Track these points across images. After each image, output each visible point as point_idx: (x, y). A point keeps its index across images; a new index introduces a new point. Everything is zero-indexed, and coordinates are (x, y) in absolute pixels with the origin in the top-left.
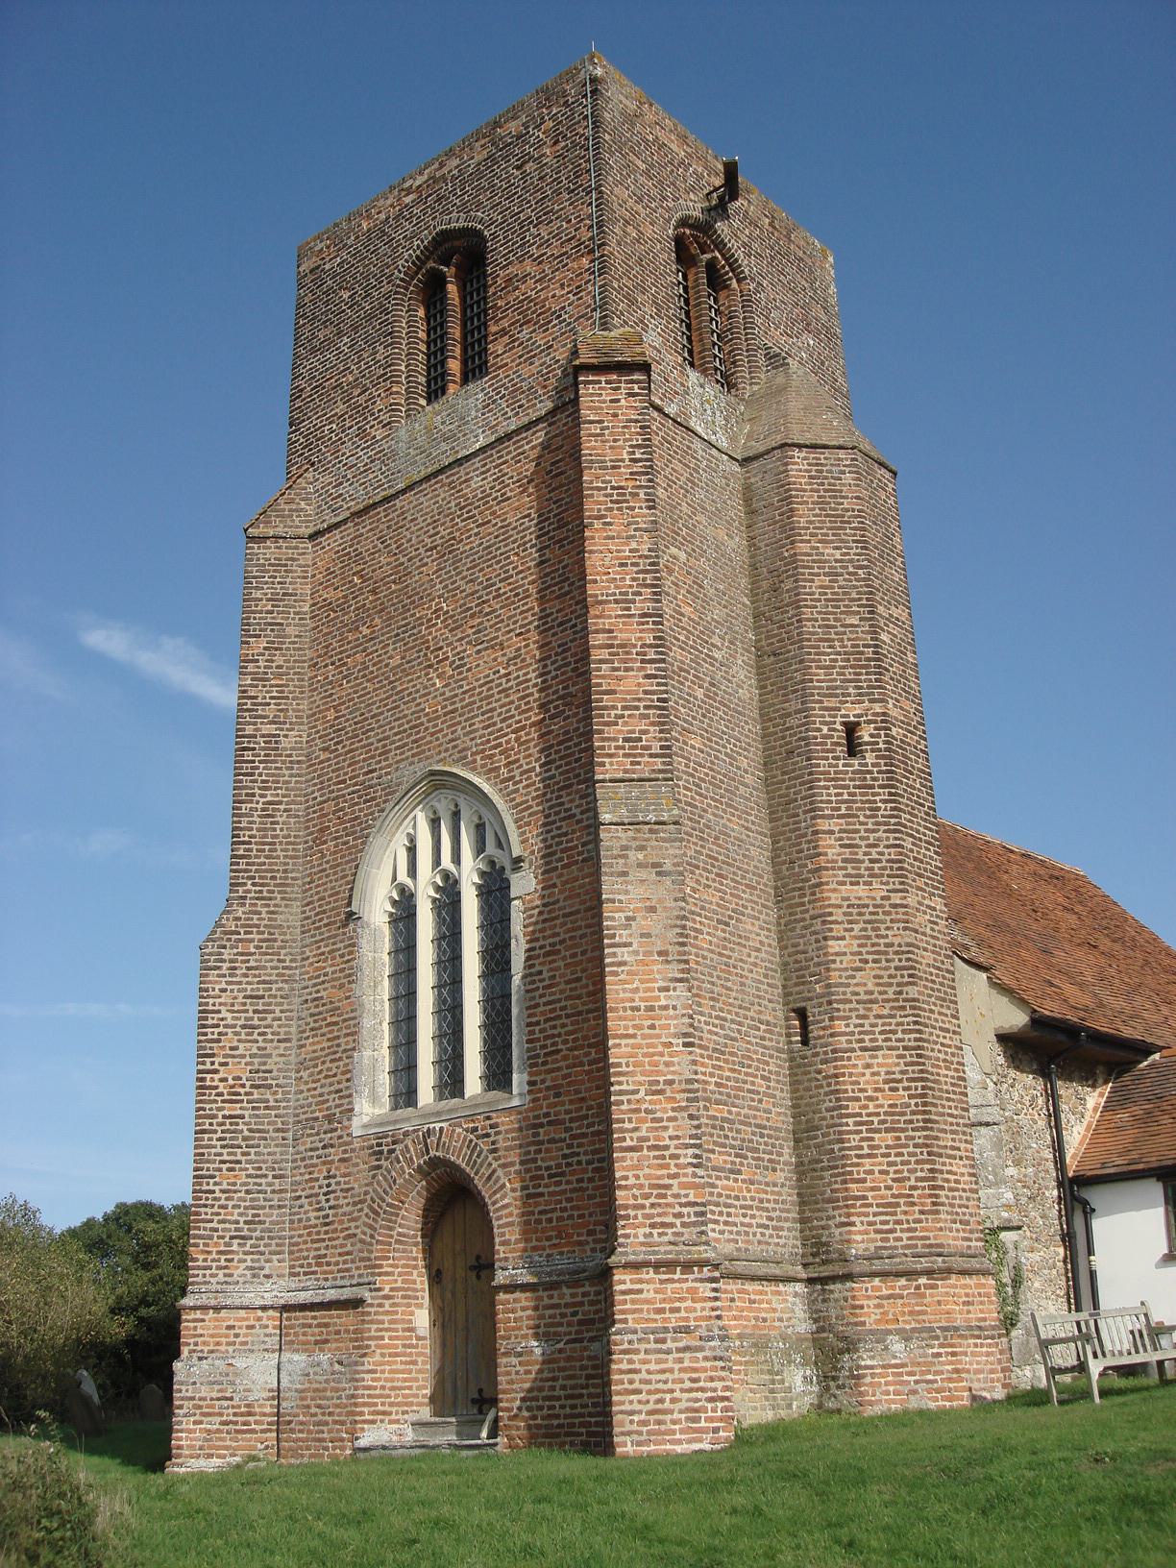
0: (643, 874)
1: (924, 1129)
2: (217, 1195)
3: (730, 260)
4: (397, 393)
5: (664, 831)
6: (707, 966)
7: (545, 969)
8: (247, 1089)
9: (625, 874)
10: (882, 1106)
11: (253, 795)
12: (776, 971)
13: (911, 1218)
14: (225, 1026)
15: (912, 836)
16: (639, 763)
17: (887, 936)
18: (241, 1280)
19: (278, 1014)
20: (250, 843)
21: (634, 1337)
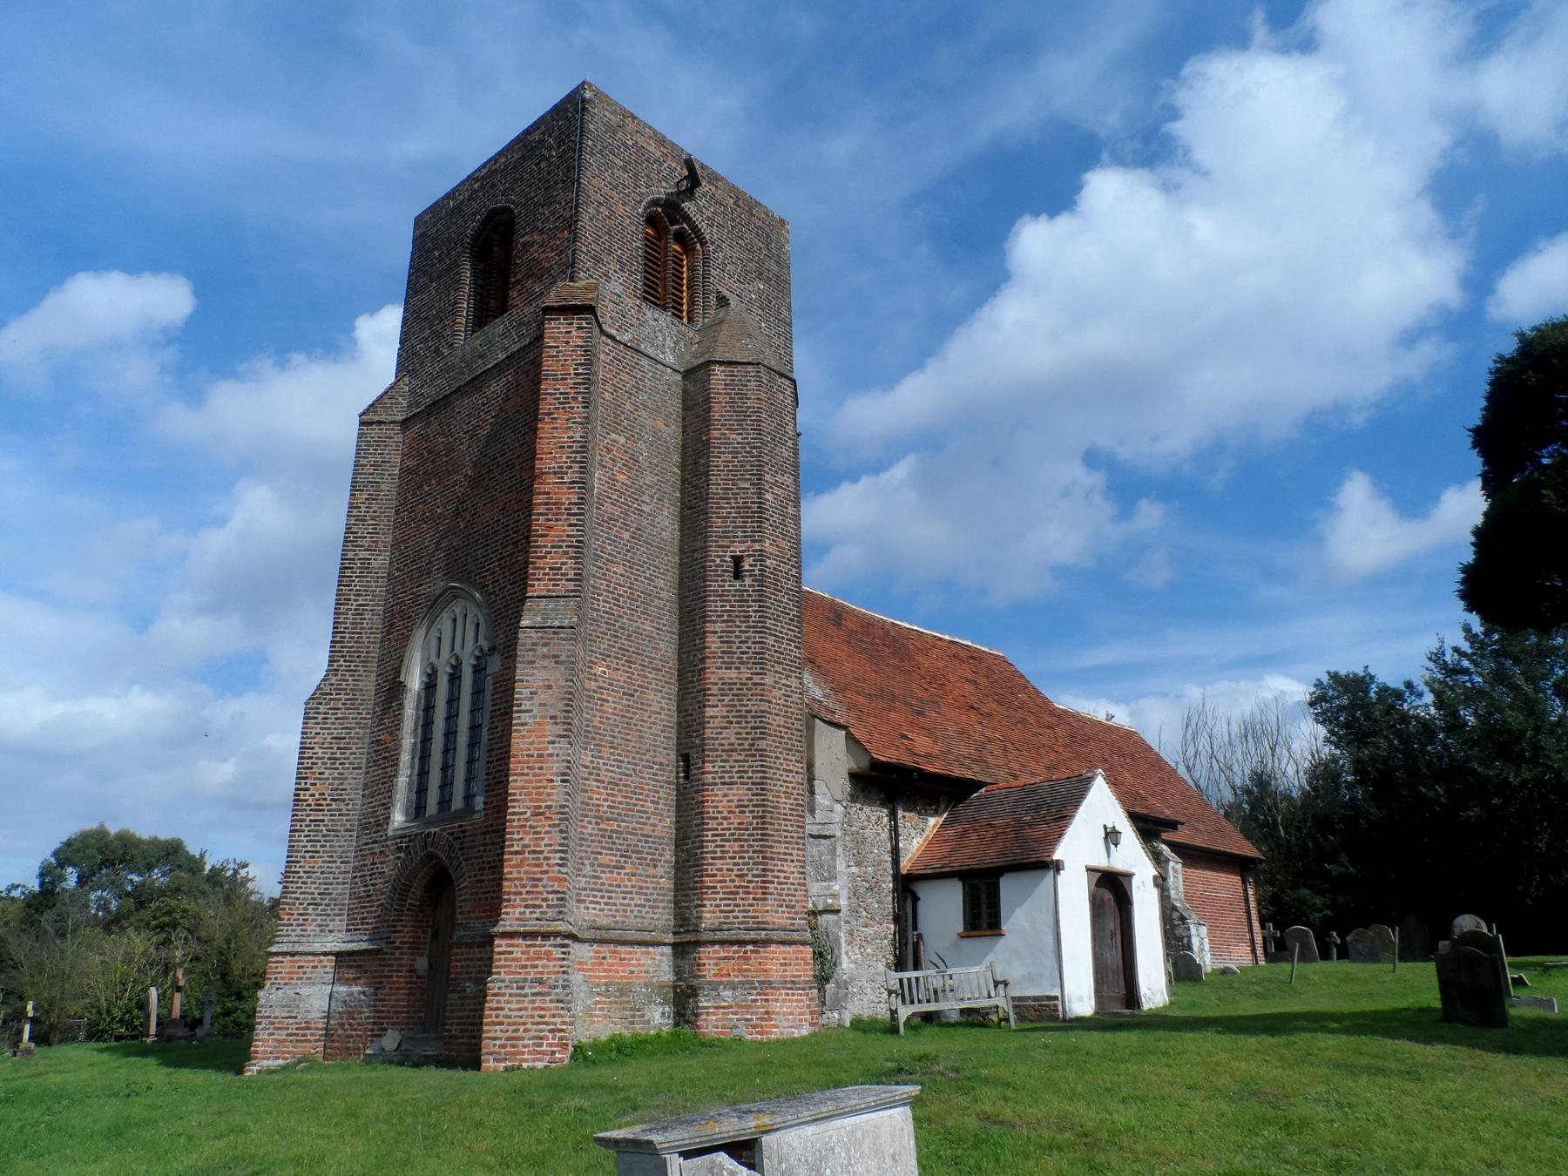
0: (545, 663)
1: (761, 840)
2: (301, 874)
3: (694, 227)
4: (459, 323)
5: (564, 633)
6: (610, 725)
7: (499, 725)
8: (328, 802)
9: (532, 662)
10: (733, 824)
11: (350, 600)
12: (673, 728)
13: (746, 903)
14: (317, 758)
15: (775, 635)
16: (558, 585)
17: (747, 705)
18: (312, 933)
19: (354, 750)
20: (344, 632)
21: (503, 984)
